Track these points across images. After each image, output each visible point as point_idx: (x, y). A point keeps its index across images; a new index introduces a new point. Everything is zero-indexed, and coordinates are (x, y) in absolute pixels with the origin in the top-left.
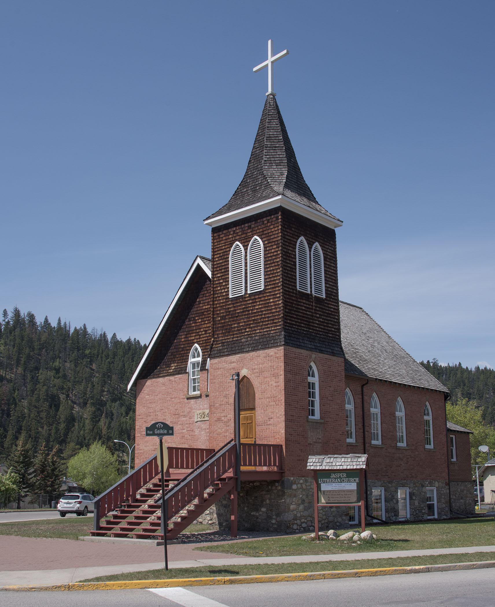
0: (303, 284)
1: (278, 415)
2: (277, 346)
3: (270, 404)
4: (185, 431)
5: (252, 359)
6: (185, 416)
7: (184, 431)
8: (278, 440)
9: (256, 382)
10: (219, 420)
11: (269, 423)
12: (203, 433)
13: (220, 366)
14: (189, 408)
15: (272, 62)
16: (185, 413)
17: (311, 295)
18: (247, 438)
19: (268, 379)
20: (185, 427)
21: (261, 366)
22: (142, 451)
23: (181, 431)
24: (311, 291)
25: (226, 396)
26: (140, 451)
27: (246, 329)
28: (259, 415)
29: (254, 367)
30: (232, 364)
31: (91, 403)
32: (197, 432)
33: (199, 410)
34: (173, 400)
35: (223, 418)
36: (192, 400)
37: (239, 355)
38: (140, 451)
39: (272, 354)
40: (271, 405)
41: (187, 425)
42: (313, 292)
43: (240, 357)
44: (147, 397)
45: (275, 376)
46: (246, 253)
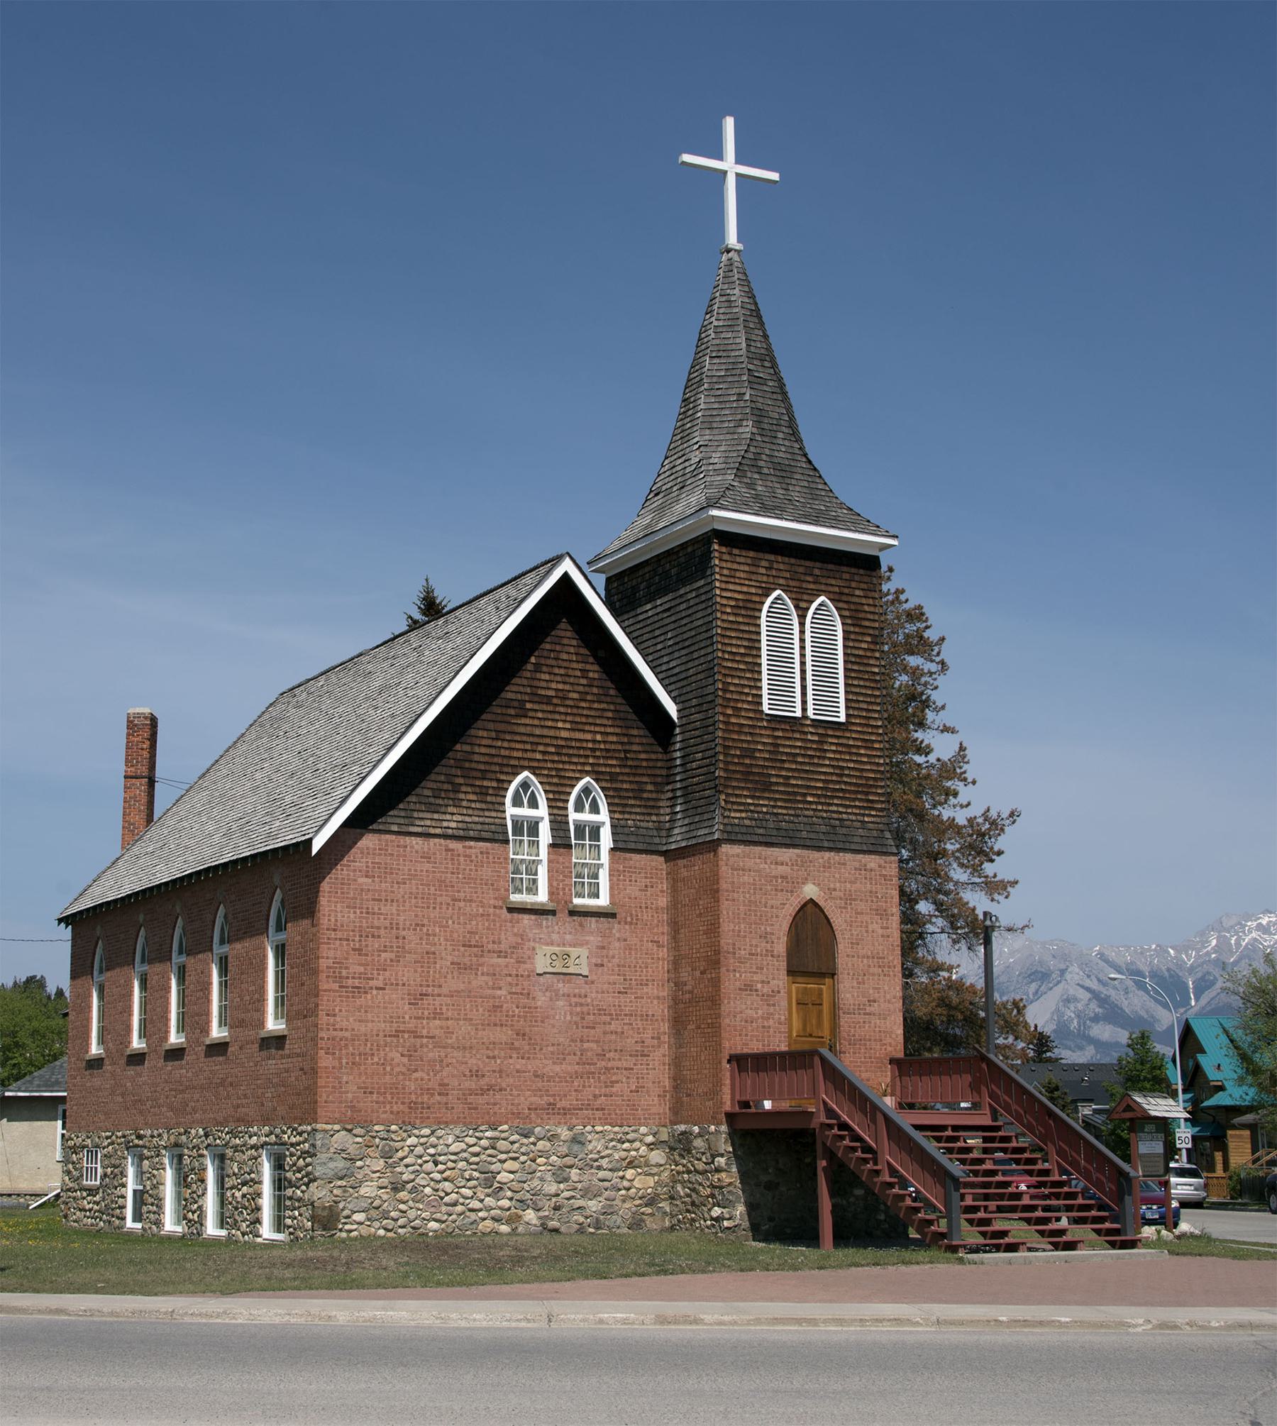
0: (783, 690)
1: (888, 997)
2: (885, 854)
3: (871, 970)
4: (503, 992)
5: (827, 866)
6: (500, 954)
7: (499, 992)
8: (889, 1049)
9: (838, 920)
10: (748, 988)
11: (868, 1009)
12: (561, 1003)
13: (750, 863)
14: (515, 935)
15: (739, 161)
16: (503, 947)
17: (805, 717)
18: (811, 1035)
19: (865, 918)
20: (502, 984)
21: (848, 885)
22: (347, 1034)
23: (490, 992)
24: (804, 710)
25: (764, 936)
26: (340, 1034)
27: (805, 795)
28: (848, 990)
29: (832, 886)
30: (780, 867)
31: (1213, 983)
32: (542, 1000)
33: (547, 944)
34: (462, 904)
35: (759, 986)
36: (526, 917)
37: (796, 851)
38: (340, 1034)
39: (872, 865)
40: (873, 975)
41: (509, 979)
42: (810, 713)
43: (798, 856)
44: (361, 880)
45: (883, 914)
46: (802, 624)
